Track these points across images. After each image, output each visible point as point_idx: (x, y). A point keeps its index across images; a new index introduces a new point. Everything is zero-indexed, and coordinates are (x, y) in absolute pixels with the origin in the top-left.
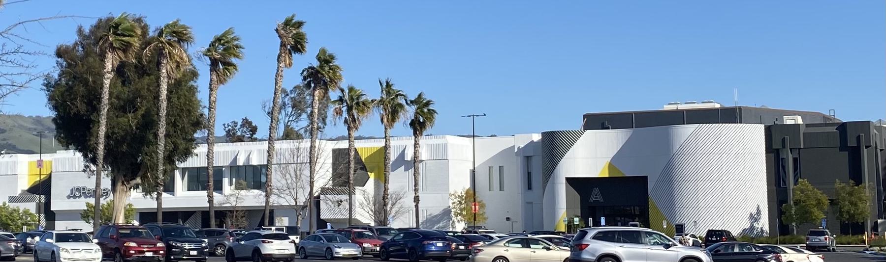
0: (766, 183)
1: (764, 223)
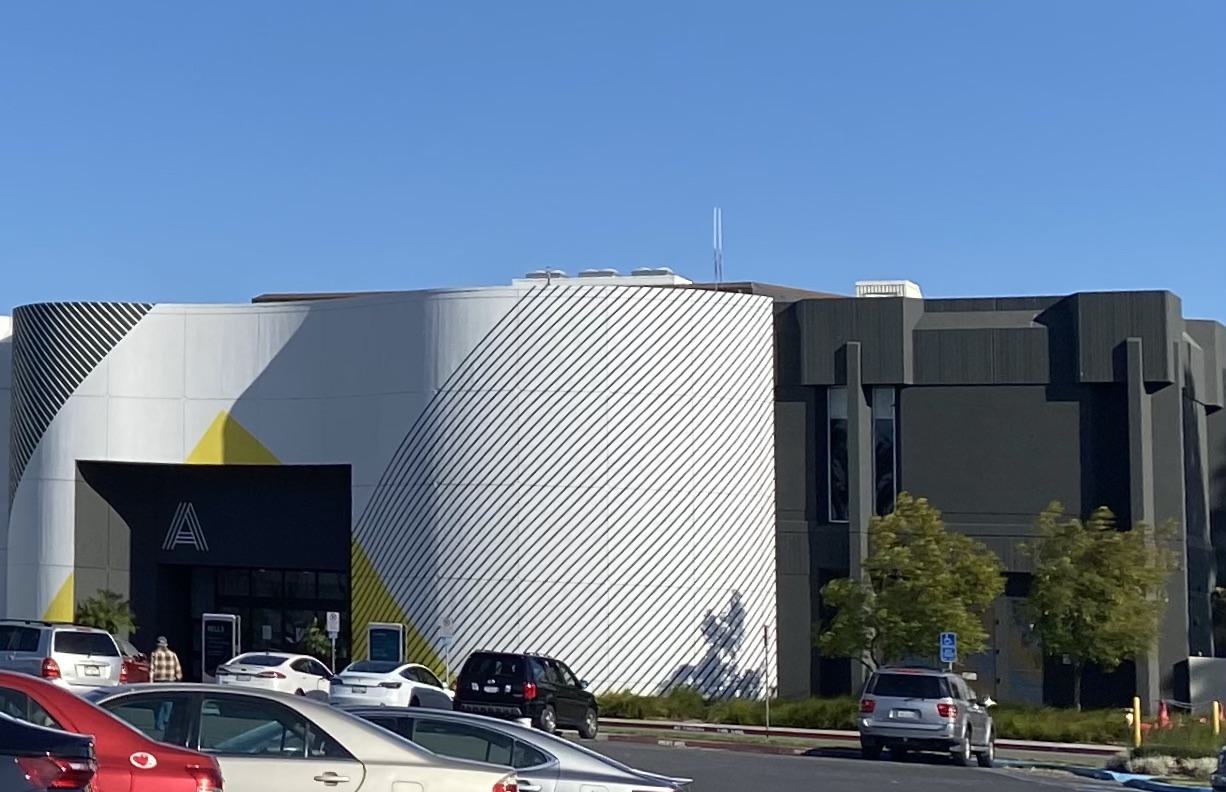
0: (771, 509)
1: (757, 654)
